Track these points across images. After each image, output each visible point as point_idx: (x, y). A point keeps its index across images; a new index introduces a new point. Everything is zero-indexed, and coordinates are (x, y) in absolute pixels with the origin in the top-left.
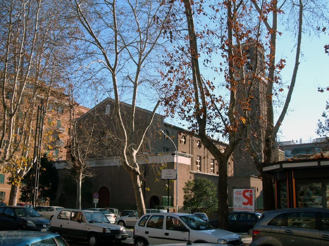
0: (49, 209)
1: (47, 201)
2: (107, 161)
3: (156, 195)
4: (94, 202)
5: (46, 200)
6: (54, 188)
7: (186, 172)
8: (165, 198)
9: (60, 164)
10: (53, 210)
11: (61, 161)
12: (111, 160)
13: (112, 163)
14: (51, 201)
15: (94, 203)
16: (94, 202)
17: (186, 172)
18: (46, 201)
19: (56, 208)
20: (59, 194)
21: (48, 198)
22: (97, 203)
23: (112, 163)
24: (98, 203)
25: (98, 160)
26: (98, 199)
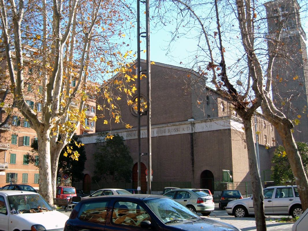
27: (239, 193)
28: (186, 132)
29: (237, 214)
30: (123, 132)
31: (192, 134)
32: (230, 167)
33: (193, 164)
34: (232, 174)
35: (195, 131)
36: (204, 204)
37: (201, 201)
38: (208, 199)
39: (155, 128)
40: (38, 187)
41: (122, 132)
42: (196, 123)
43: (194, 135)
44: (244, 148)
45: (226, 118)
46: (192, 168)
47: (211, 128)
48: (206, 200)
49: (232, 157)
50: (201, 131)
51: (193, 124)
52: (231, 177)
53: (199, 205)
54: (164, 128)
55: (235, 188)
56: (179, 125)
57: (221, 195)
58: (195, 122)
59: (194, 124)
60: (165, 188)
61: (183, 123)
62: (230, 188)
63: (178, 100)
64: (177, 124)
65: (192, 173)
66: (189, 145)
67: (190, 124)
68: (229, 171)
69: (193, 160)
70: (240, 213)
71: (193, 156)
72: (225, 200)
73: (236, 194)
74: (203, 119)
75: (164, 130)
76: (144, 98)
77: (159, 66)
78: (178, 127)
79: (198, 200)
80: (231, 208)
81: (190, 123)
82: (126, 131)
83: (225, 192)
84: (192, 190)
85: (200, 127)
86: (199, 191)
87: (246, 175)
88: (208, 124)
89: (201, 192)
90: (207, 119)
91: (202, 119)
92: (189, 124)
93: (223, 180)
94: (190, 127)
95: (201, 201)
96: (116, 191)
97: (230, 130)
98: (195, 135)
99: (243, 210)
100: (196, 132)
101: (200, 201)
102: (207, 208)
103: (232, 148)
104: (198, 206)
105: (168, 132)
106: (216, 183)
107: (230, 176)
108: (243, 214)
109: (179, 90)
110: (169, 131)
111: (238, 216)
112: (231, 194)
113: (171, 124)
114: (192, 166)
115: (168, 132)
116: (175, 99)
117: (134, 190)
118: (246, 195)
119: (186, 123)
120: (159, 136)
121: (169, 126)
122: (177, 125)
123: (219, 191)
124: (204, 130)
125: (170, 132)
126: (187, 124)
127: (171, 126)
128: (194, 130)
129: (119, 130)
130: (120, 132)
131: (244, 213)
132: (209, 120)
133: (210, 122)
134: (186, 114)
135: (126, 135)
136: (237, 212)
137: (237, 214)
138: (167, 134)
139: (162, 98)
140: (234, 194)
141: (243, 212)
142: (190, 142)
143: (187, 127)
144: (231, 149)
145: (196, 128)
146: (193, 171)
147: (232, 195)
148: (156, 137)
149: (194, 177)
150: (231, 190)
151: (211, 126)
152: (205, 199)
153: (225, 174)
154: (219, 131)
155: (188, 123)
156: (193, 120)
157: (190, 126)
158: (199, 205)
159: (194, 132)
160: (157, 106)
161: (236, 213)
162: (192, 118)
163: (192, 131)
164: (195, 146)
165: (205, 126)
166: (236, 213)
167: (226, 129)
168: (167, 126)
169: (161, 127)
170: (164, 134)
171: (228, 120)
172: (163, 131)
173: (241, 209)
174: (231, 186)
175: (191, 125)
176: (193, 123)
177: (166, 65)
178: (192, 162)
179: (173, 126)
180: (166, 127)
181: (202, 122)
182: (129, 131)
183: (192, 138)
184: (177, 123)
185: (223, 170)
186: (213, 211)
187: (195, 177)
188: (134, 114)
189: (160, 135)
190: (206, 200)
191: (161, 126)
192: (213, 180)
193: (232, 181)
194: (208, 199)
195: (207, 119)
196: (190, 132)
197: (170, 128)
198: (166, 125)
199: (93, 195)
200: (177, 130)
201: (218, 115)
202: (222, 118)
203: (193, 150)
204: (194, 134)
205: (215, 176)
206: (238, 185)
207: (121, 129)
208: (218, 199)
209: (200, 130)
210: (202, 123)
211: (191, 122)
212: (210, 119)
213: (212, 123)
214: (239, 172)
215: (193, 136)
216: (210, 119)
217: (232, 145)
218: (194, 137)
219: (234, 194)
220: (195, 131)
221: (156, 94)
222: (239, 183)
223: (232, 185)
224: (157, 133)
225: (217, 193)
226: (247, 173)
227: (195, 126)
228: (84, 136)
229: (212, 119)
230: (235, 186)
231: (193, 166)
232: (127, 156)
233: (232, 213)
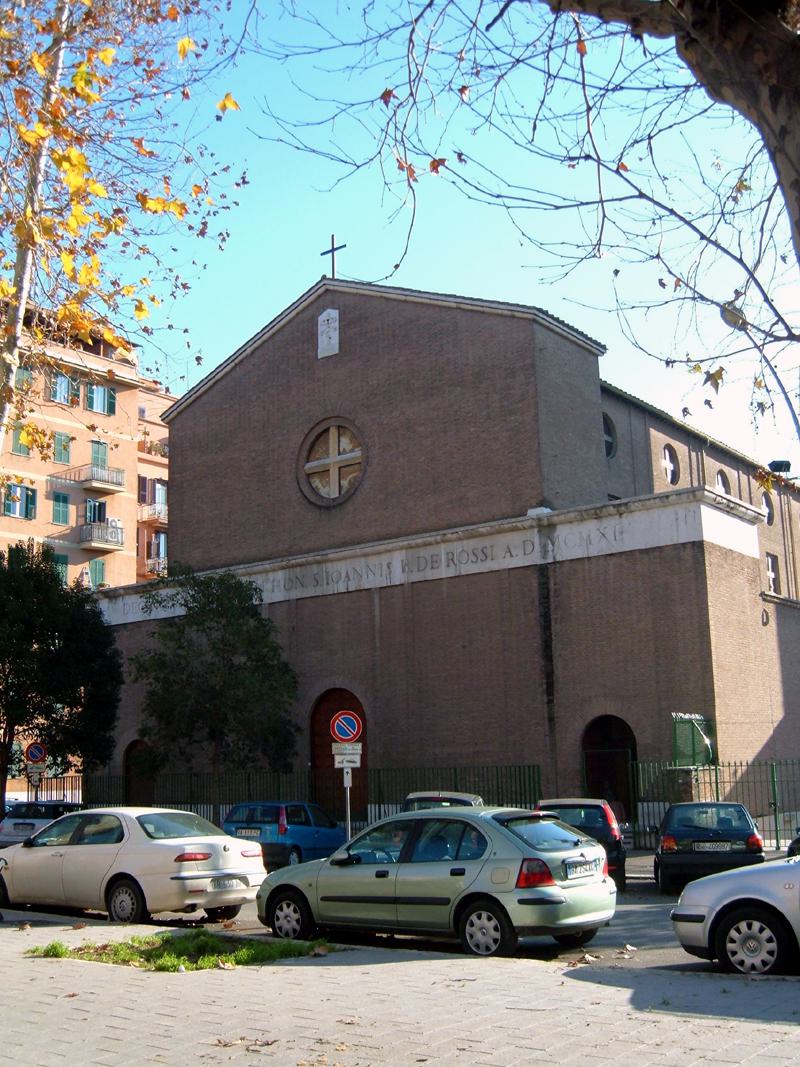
0: (90, 829)
1: (72, 773)
2: (342, 567)
3: (611, 709)
4: (337, 765)
5: (67, 766)
6: (102, 709)
7: (746, 590)
8: (690, 721)
9: (120, 602)
10: (115, 834)
11: (122, 591)
12: (363, 560)
13: (371, 576)
14: (86, 771)
15: (342, 770)
16: (337, 765)
17: (746, 590)
18: (65, 771)
19: (141, 820)
20: (126, 731)
21: (76, 760)
22: (353, 769)
23: (371, 576)
24: (358, 765)
25: (298, 569)
26: (359, 746)
27: (742, 816)
28: (519, 561)
29: (734, 953)
30: (274, 570)
31: (543, 571)
32: (705, 701)
33: (550, 689)
34: (710, 728)
35: (554, 558)
36: (554, 890)
37: (537, 873)
38: (576, 865)
39: (397, 550)
40: (22, 790)
41: (266, 572)
42: (562, 523)
43: (551, 573)
44: (761, 622)
45: (684, 497)
46: (546, 706)
47: (622, 540)
48: (566, 867)
49: (707, 614)
50: (580, 556)
51: (547, 528)
52: (707, 741)
53: (526, 894)
54: (431, 550)
55: (728, 789)
56: (491, 534)
57: (661, 826)
58: (555, 519)
59: (552, 526)
60: (411, 796)
61: (506, 524)
62: (704, 794)
63: (484, 435)
64: (481, 530)
65: (547, 728)
66: (534, 615)
67: (536, 530)
68: (698, 716)
69: (549, 676)
70: (752, 944)
71: (552, 661)
72: (678, 852)
73: (730, 820)
74: (588, 507)
75: (429, 558)
76: (353, 433)
77: (406, 301)
78: (487, 542)
79: (525, 870)
80: (700, 919)
81: (534, 524)
82: (283, 568)
83: (678, 814)
84: (495, 818)
85: (577, 541)
86: (539, 818)
87: (772, 732)
88: (611, 524)
89: (542, 822)
90: (605, 506)
91: (584, 508)
92: (532, 527)
93: (674, 754)
94: (537, 540)
95: (537, 873)
96: (138, 818)
97: (699, 546)
98: (555, 572)
99: (767, 933)
100: (559, 559)
101: (534, 874)
102: (572, 912)
103: (711, 623)
104: (522, 902)
105: (448, 566)
106: (648, 772)
107: (702, 740)
108: (771, 953)
109: (488, 394)
110: (451, 560)
111: (742, 963)
112: (709, 819)
113: (457, 530)
114: (545, 699)
115: (448, 566)
116: (472, 429)
117: (283, 806)
118: (773, 817)
119: (519, 524)
120: (413, 583)
121: (450, 541)
122: (481, 535)
123: (653, 801)
124: (594, 551)
125: (456, 565)
126: (525, 528)
127: (460, 539)
128: (551, 553)
129: (256, 564)
130: (260, 573)
131: (773, 946)
132: (611, 508)
133: (617, 517)
134: (518, 491)
135: (282, 582)
136: (733, 941)
137: (734, 953)
138: (444, 572)
139: (422, 429)
140: (721, 821)
141: (770, 940)
142: (537, 603)
143: (524, 542)
144: (708, 626)
145: (562, 544)
146: (551, 719)
147: (715, 826)
148: (402, 585)
149: (553, 745)
150: (708, 801)
151: (622, 533)
152: (563, 861)
153: (682, 733)
154: (656, 554)
155: (527, 524)
156: (546, 511)
157: (534, 536)
158: (526, 894)
159: (550, 560)
160: (401, 460)
161: (730, 946)
162: (542, 503)
163: (544, 557)
164: (556, 619)
165: (595, 535)
166: (730, 946)
167: (684, 544)
168: (443, 541)
169: (418, 546)
170: (430, 575)
171: (692, 507)
172: (425, 559)
173: (756, 925)
174: (707, 779)
175: (539, 531)
176: (545, 522)
177: (444, 298)
178: (547, 683)
179: (468, 538)
180: (437, 543)
181: (582, 520)
182: (293, 566)
183: (544, 587)
184: (483, 528)
185: (674, 714)
186: (607, 924)
187: (559, 745)
188: (313, 499)
189: (416, 577)
190: (566, 867)
191: (419, 541)
192: (635, 757)
193: (712, 759)
194: (576, 865)
195: (605, 506)
196: (536, 559)
197: (457, 547)
198: (439, 538)
199: (40, 841)
200: (481, 556)
201: (651, 488)
202: (667, 497)
203: (551, 634)
204: (551, 568)
205: (643, 738)
206: (739, 774)
207: (265, 559)
208: (648, 837)
209: (578, 553)
210: (585, 523)
211: (539, 520)
212: (614, 506)
213: (626, 519)
214: (741, 723)
215: (548, 578)
216: (614, 506)
217: (711, 609)
218: (552, 582)
219: (721, 821)
220: (554, 558)
221: (396, 413)
222: (744, 768)
223: (713, 779)
224: (403, 571)
225: (657, 810)
226: (775, 725)
227: (555, 535)
228: (127, 594)
229: (626, 504)
230: (727, 779)
231: (550, 702)
232: (276, 662)
233: (704, 942)
